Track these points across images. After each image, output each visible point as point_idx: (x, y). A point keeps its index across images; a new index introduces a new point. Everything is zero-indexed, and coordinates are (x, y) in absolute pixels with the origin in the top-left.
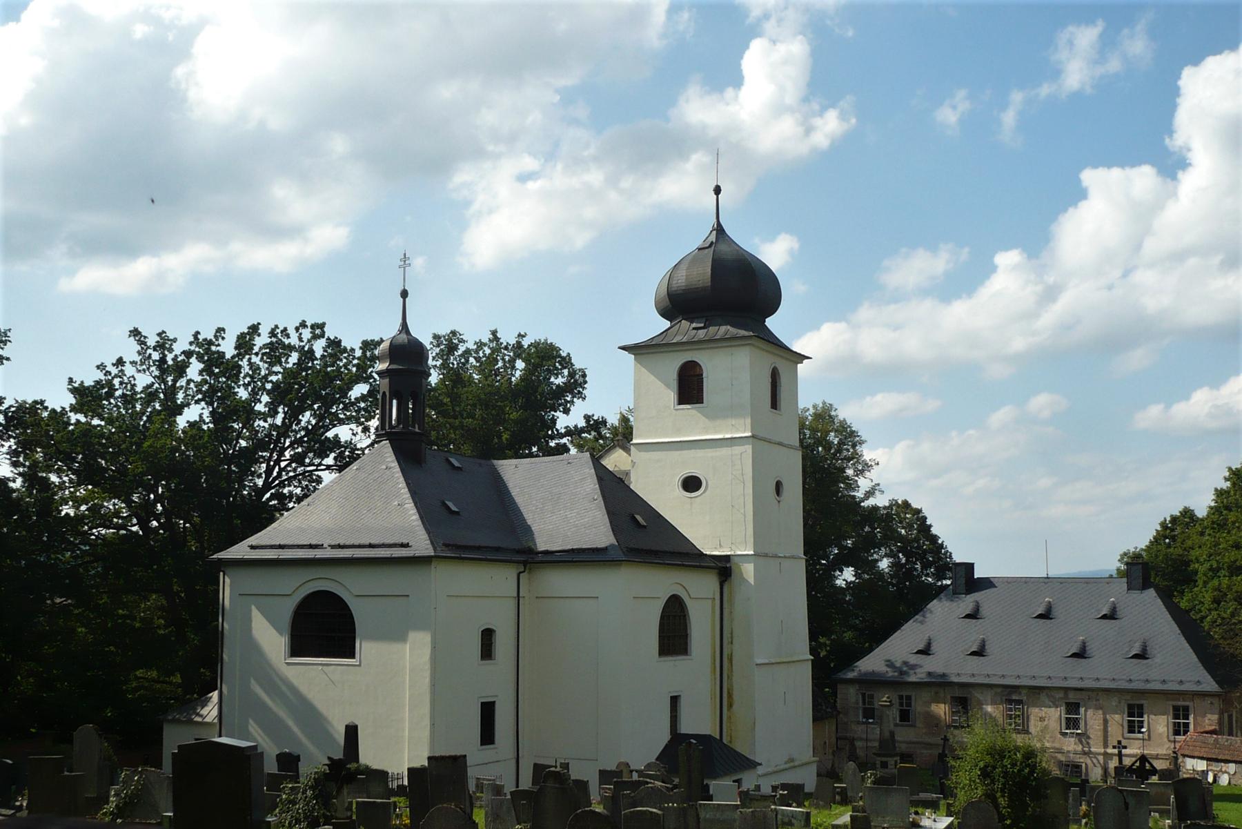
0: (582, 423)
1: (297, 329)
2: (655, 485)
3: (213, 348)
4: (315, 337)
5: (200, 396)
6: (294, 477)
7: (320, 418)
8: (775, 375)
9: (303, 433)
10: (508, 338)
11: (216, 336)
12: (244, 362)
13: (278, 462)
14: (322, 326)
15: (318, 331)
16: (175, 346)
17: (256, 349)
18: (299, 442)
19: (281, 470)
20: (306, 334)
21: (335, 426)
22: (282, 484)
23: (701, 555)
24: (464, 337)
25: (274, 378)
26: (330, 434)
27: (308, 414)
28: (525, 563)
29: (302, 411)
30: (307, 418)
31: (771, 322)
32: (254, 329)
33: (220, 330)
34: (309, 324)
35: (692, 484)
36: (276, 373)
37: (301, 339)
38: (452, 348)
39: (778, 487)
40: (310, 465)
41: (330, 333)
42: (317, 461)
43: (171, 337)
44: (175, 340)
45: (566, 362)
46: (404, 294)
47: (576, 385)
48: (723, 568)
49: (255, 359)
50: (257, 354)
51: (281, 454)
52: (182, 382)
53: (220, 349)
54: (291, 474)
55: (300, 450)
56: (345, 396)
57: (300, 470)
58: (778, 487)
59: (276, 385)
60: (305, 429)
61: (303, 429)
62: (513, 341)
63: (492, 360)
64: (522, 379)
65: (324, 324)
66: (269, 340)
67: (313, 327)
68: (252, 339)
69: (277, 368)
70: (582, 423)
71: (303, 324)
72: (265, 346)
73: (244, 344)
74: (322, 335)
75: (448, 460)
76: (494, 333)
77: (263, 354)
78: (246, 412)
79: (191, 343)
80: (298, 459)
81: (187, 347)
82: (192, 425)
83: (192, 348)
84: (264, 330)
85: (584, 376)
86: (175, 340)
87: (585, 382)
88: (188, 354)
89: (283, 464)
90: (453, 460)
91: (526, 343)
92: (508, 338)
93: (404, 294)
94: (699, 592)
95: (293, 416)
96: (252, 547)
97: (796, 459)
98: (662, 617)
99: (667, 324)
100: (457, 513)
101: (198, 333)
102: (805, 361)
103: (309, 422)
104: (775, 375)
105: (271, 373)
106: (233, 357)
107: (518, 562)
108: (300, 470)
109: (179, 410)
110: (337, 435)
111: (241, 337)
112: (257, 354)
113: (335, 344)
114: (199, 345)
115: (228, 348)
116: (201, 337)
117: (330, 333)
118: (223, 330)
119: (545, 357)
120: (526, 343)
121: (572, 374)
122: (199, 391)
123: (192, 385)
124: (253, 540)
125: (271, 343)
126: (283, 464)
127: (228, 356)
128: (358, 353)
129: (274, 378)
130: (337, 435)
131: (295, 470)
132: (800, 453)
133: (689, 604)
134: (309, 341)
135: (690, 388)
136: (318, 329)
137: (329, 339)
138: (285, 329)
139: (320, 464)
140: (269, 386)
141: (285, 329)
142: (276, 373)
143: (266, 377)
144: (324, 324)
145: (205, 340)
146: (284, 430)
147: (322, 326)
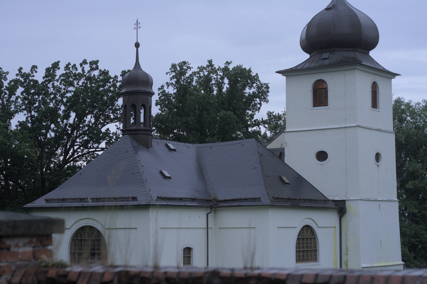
0: (266, 118)
1: (81, 65)
2: (299, 158)
3: (30, 78)
4: (92, 69)
5: (24, 107)
6: (82, 155)
7: (97, 118)
8: (375, 86)
9: (86, 128)
10: (219, 64)
11: (31, 70)
12: (50, 85)
13: (72, 146)
14: (96, 62)
15: (94, 66)
16: (7, 76)
17: (57, 78)
18: (84, 133)
19: (74, 151)
20: (87, 68)
21: (108, 123)
22: (75, 160)
23: (327, 200)
24: (191, 66)
25: (69, 95)
26: (103, 130)
27: (89, 116)
28: (211, 208)
29: (86, 115)
30: (89, 119)
31: (372, 53)
32: (56, 65)
33: (34, 68)
34: (88, 62)
35: (322, 156)
36: (70, 92)
37: (83, 70)
38: (182, 73)
39: (378, 157)
40: (91, 148)
41: (102, 66)
42: (95, 145)
43: (5, 71)
44: (8, 73)
45: (255, 79)
46: (137, 45)
47: (263, 93)
48: (340, 208)
49: (56, 84)
50: (57, 81)
51: (74, 141)
52: (13, 98)
53: (35, 78)
54: (80, 154)
55: (86, 138)
56: (113, 105)
57: (86, 151)
58: (378, 157)
59: (69, 100)
60: (88, 125)
61: (87, 126)
62: (222, 66)
63: (208, 79)
64: (228, 91)
65: (98, 61)
66: (65, 72)
67: (90, 63)
68: (54, 71)
69: (71, 88)
70: (266, 118)
71: (85, 62)
72: (63, 75)
73: (50, 73)
74: (97, 68)
75: (167, 145)
76: (210, 62)
77: (62, 80)
78: (52, 115)
79: (17, 75)
80: (85, 145)
81: (14, 77)
82: (21, 124)
83: (18, 78)
84: (62, 66)
85: (268, 87)
86: (8, 73)
87: (268, 92)
88: (16, 82)
89: (76, 148)
90: (169, 145)
91: (231, 67)
92: (219, 64)
93: (137, 45)
94: (324, 224)
95: (81, 117)
96: (47, 200)
97: (392, 139)
98: (298, 239)
99: (307, 56)
100: (170, 178)
101: (21, 68)
102: (397, 77)
103: (90, 122)
104: (375, 86)
105: (68, 92)
106: (42, 83)
107: (207, 207)
108: (86, 151)
109: (11, 115)
110: (108, 129)
111: (48, 70)
112: (57, 81)
113: (105, 73)
114: (22, 76)
115: (39, 77)
116: (23, 71)
117: (102, 66)
118: (36, 67)
119: (241, 77)
120: (231, 67)
121: (259, 88)
122: (23, 104)
123: (19, 100)
124: (48, 196)
125: (66, 73)
126: (76, 148)
127: (40, 83)
128: (120, 78)
129: (69, 95)
130: (108, 129)
131: (82, 151)
132: (394, 135)
133: (319, 233)
134: (89, 72)
135: (320, 96)
136: (94, 64)
137: (100, 71)
138: (75, 65)
139: (98, 147)
140: (65, 100)
141: (75, 65)
142: (70, 92)
143: (64, 93)
144: (98, 61)
145: (25, 73)
146: (75, 127)
147: (96, 62)
